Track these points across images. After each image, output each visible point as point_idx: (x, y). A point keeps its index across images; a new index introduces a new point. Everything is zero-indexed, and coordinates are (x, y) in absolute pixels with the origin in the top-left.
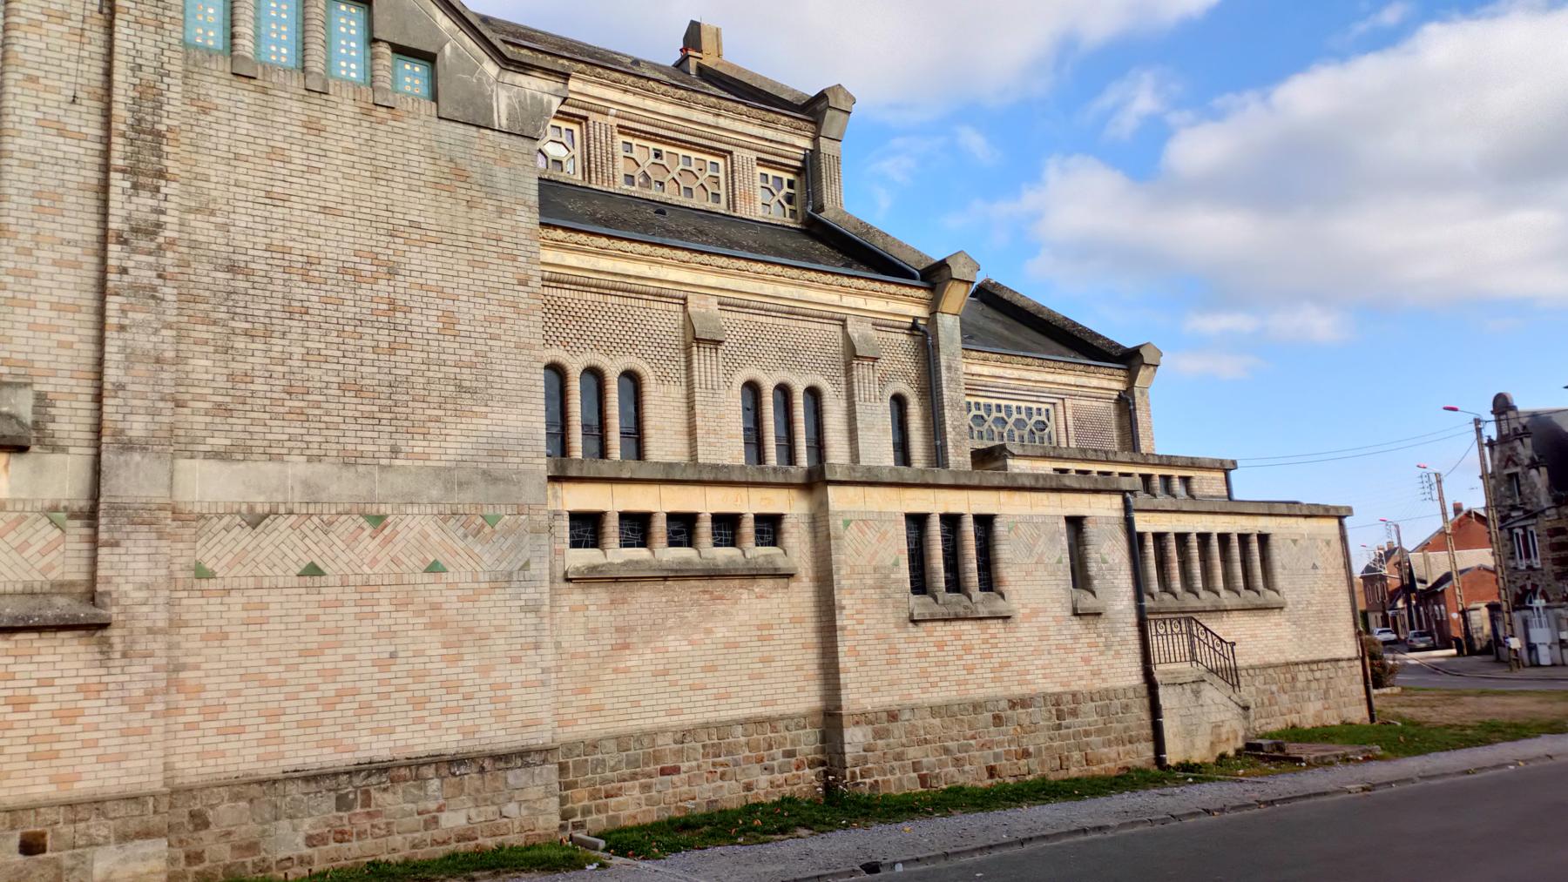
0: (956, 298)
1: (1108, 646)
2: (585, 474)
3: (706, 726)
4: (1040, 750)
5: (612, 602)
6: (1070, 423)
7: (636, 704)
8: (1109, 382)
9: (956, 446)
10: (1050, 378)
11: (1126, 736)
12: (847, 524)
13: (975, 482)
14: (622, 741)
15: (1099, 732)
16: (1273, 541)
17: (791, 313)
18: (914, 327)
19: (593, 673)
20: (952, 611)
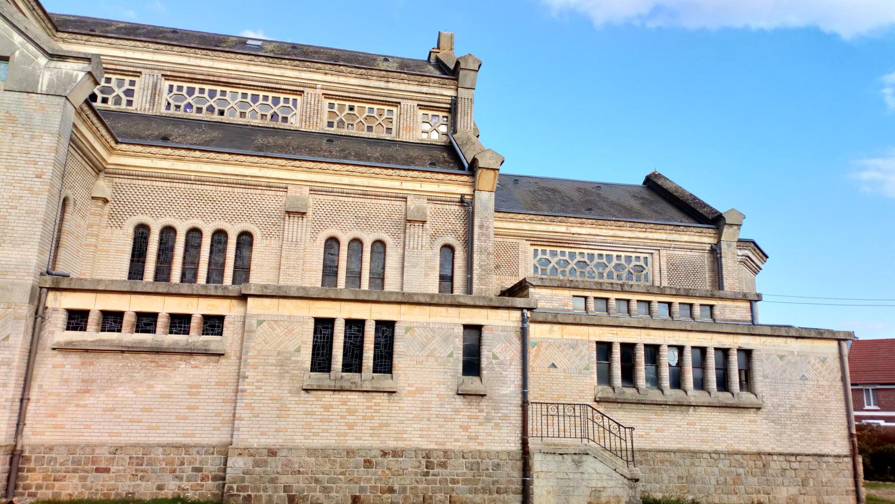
0: (486, 180)
1: (488, 419)
2: (72, 287)
3: (134, 446)
4: (404, 490)
5: (83, 364)
6: (664, 267)
7: (87, 427)
8: (707, 238)
9: (480, 279)
10: (643, 235)
11: (494, 488)
12: (260, 323)
13: (375, 298)
14: (71, 449)
15: (466, 481)
16: (755, 355)
17: (365, 195)
18: (462, 201)
19: (61, 405)
20: (338, 385)
